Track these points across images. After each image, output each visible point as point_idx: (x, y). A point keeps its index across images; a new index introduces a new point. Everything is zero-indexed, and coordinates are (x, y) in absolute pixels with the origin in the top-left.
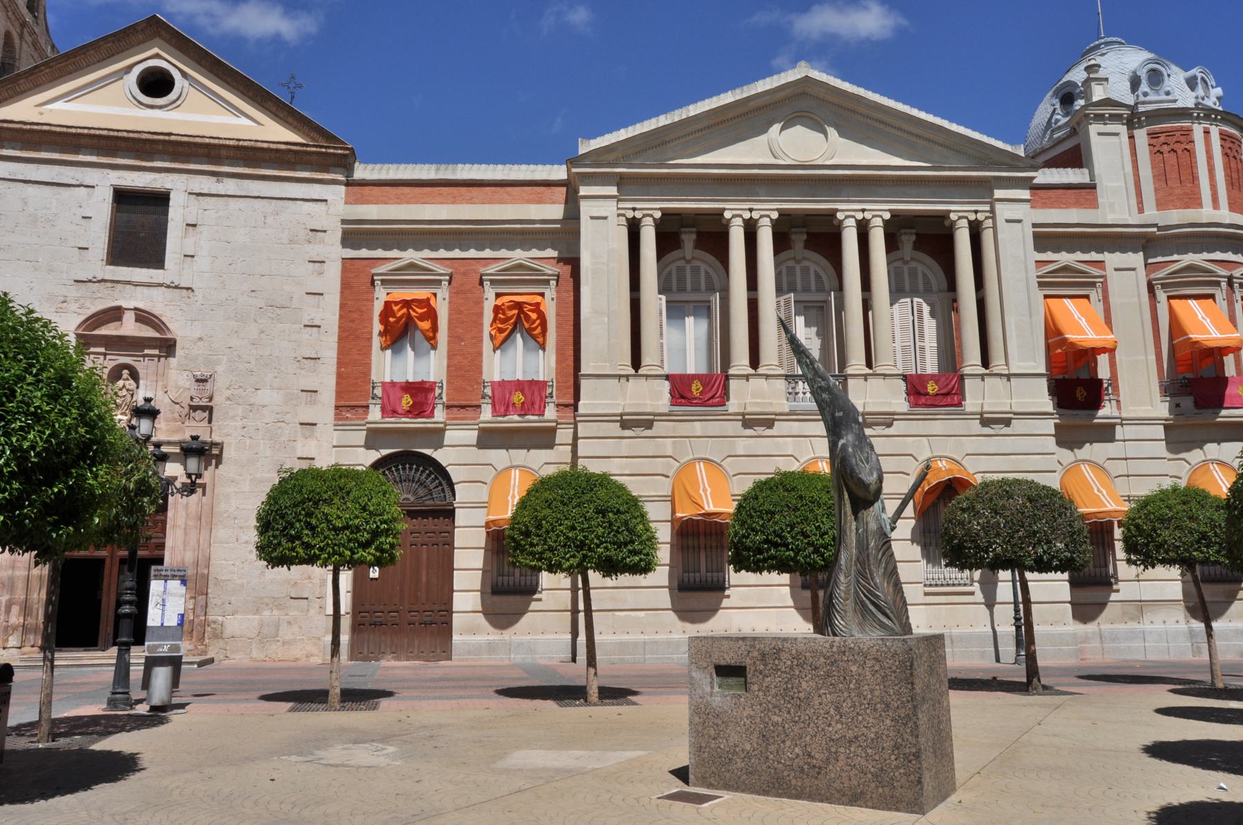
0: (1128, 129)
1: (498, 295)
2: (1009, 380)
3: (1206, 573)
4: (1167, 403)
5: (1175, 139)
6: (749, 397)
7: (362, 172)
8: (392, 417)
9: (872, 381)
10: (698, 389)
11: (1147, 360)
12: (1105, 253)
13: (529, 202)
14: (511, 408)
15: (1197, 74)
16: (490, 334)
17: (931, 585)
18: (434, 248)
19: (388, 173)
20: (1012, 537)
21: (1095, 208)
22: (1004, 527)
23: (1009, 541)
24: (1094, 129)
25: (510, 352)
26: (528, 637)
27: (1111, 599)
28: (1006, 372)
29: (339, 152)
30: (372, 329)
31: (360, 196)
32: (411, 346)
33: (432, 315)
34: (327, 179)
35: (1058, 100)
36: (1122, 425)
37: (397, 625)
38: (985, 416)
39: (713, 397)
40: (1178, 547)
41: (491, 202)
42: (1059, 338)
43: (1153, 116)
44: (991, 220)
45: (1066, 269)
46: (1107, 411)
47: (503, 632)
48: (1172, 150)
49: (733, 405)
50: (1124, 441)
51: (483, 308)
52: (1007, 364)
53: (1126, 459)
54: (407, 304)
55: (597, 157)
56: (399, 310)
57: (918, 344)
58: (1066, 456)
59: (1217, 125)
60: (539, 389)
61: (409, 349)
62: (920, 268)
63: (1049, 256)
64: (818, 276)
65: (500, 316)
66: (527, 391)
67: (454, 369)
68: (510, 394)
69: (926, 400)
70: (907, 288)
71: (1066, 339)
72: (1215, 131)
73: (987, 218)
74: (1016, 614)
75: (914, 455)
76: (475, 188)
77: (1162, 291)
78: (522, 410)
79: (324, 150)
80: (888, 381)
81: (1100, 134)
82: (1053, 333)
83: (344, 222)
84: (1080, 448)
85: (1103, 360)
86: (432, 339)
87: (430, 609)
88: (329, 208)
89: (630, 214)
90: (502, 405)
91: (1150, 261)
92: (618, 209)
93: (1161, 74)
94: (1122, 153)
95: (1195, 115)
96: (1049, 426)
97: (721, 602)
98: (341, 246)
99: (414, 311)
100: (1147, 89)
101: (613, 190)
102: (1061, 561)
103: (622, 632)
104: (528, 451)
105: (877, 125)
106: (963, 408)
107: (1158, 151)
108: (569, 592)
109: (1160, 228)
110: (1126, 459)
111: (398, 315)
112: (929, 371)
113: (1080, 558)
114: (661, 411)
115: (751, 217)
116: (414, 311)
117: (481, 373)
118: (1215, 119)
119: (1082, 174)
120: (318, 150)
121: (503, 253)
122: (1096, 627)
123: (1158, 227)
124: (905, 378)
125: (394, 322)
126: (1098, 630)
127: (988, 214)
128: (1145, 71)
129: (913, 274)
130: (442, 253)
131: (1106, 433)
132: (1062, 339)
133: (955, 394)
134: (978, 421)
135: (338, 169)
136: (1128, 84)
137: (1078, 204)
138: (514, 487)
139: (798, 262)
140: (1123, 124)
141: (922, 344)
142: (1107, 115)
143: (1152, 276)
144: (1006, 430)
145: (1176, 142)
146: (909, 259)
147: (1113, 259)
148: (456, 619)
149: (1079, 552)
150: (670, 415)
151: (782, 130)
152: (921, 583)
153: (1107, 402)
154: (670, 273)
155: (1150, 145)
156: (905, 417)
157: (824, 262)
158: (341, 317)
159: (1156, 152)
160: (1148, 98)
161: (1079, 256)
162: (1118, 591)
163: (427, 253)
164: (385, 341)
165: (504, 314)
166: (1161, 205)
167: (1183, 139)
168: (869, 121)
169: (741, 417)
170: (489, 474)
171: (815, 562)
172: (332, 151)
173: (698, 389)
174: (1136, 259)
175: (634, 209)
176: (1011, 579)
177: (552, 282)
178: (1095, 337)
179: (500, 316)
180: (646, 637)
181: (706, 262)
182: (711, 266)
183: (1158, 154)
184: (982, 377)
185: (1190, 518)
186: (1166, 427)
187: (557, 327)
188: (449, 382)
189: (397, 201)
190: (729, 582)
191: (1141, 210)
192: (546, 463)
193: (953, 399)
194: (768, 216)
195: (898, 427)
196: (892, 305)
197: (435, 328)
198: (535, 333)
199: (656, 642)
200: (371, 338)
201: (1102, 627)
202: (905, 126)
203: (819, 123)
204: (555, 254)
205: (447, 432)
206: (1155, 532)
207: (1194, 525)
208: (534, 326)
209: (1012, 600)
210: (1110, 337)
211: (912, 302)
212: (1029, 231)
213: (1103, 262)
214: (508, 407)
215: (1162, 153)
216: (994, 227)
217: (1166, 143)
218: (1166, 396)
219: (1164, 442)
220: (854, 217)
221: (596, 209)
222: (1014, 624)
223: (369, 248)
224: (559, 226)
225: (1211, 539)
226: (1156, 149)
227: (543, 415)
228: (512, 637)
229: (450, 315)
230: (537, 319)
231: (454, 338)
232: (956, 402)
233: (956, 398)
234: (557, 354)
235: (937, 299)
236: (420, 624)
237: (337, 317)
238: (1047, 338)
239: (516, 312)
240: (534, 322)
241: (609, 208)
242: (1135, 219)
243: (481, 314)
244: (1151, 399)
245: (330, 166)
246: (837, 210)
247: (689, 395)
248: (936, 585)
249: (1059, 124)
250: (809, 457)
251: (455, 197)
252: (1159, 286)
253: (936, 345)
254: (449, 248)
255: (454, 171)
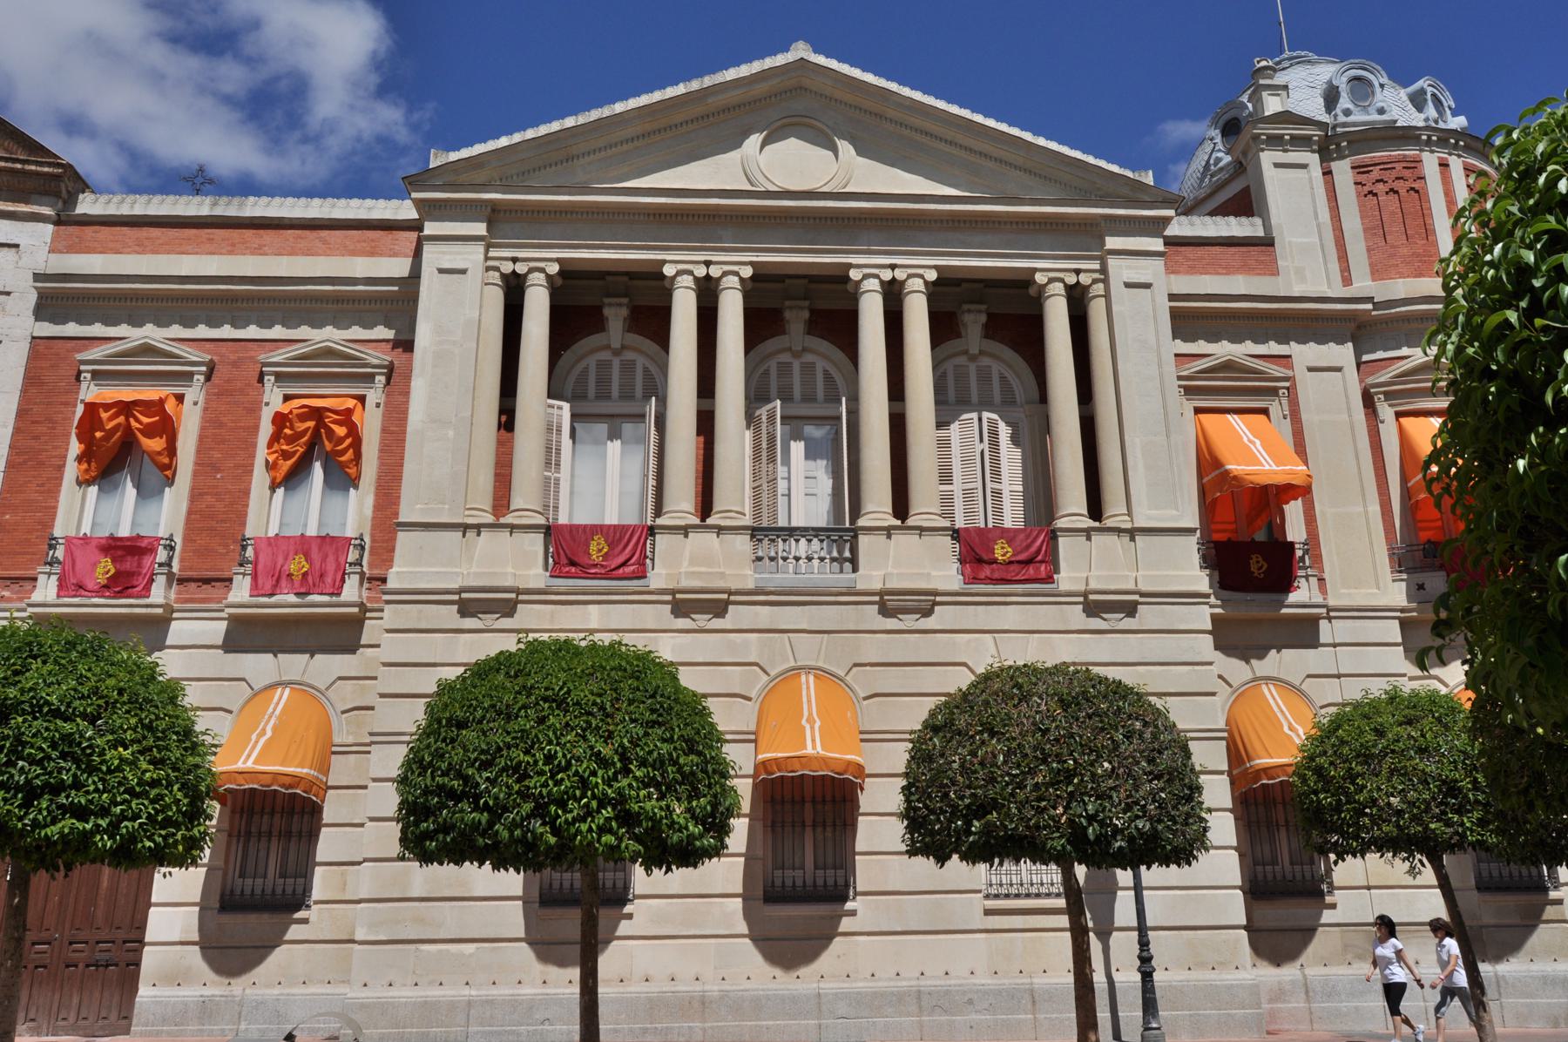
0: (1322, 161)
1: (287, 398)
2: (1133, 539)
3: (1485, 874)
4: (1404, 584)
5: (1394, 174)
6: (686, 563)
7: (87, 205)
8: (75, 596)
9: (900, 539)
10: (600, 551)
11: (1366, 512)
12: (1292, 343)
13: (354, 253)
14: (284, 582)
15: (1425, 86)
16: (267, 461)
17: (997, 896)
18: (189, 323)
19: (132, 207)
20: (1021, 786)
21: (1273, 275)
22: (1005, 762)
23: (1013, 795)
24: (1268, 158)
25: (299, 496)
26: (276, 991)
27: (1323, 921)
28: (1129, 526)
29: (46, 169)
30: (67, 450)
31: (77, 240)
32: (132, 481)
33: (167, 428)
34: (23, 212)
35: (1218, 131)
36: (1330, 619)
37: (45, 967)
38: (1092, 597)
39: (624, 564)
40: (1399, 813)
41: (293, 253)
42: (1217, 472)
43: (1359, 141)
44: (1101, 286)
45: (1228, 367)
46: (1303, 594)
47: (232, 982)
48: (1392, 190)
49: (658, 577)
50: (1335, 645)
51: (260, 418)
52: (1130, 514)
53: (1339, 676)
54: (126, 408)
55: (453, 176)
56: (111, 419)
57: (989, 485)
58: (1237, 670)
59: (1459, 156)
60: (337, 550)
61: (129, 484)
62: (996, 368)
63: (1200, 347)
64: (828, 377)
65: (287, 431)
66: (315, 555)
67: (197, 519)
68: (286, 559)
69: (993, 570)
70: (975, 398)
71: (1227, 472)
72: (1456, 164)
73: (1095, 281)
74: (1142, 950)
75: (970, 664)
76: (269, 231)
77: (1385, 405)
78: (302, 585)
79: (19, 166)
80: (928, 539)
81: (1277, 165)
82: (1208, 463)
83: (38, 277)
84: (1261, 657)
85: (1293, 511)
86: (167, 472)
87: (107, 938)
88: (20, 258)
89: (507, 267)
90: (269, 579)
91: (1365, 358)
92: (487, 258)
93: (1370, 84)
94: (1313, 195)
95: (1424, 137)
96: (1202, 616)
97: (615, 927)
98: (33, 318)
99: (137, 420)
100: (1350, 106)
101: (480, 229)
102: (1131, 840)
103: (431, 983)
104: (312, 656)
105: (918, 137)
106: (1054, 586)
107: (1370, 192)
108: (740, 900)
109: (1377, 306)
110: (1339, 676)
111: (108, 428)
112: (1008, 523)
113: (1175, 833)
114: (532, 585)
115: (1078, 282)
116: (137, 420)
117: (243, 524)
118: (1456, 146)
119: (1253, 225)
120: (10, 165)
121: (304, 332)
122: (1298, 972)
123: (1374, 304)
124: (956, 534)
125: (102, 439)
126: (1300, 977)
127: (1097, 276)
128: (1344, 79)
129: (984, 376)
130: (202, 331)
131: (1303, 633)
132: (1222, 473)
133: (1042, 562)
134: (1081, 607)
135: (45, 199)
136: (1321, 101)
137: (1246, 269)
138: (270, 717)
139: (796, 355)
140: (1313, 151)
141: (996, 486)
142: (1287, 137)
143: (1370, 380)
144: (1128, 623)
145: (1397, 178)
146: (977, 352)
147: (1305, 353)
148: (149, 957)
149: (1173, 819)
150: (545, 593)
151: (764, 144)
152: (980, 891)
153: (1304, 579)
154: (767, 373)
155: (1356, 183)
156: (955, 599)
157: (838, 355)
158: (17, 431)
159: (1367, 195)
160: (1351, 119)
161: (1250, 347)
162: (1333, 906)
163: (177, 331)
164: (87, 471)
165: (292, 428)
166: (1377, 272)
167: (1407, 173)
168: (907, 132)
169: (669, 598)
170: (236, 696)
171: (538, 838)
172: (33, 168)
173: (600, 551)
174: (1344, 354)
175: (515, 260)
176: (1132, 885)
177: (378, 378)
178: (1275, 468)
179: (287, 431)
180: (473, 993)
181: (822, 357)
182: (652, 359)
183: (1370, 196)
184: (1088, 533)
185: (1422, 751)
186: (1405, 625)
187: (381, 451)
188: (187, 539)
189: (137, 248)
190: (855, 888)
191: (1347, 281)
192: (340, 678)
193: (1038, 569)
194: (736, 274)
195: (943, 616)
196: (941, 424)
197: (171, 450)
198: (343, 459)
199: (490, 1002)
200: (64, 465)
201: (1308, 971)
202: (960, 138)
203: (827, 135)
204: (389, 334)
205: (174, 624)
206: (1353, 783)
207: (1431, 768)
208: (339, 448)
209: (1135, 923)
210: (1300, 468)
211: (980, 420)
212: (1165, 305)
213: (1290, 356)
214: (278, 580)
215: (1375, 195)
216: (1107, 296)
217: (1381, 180)
218: (1400, 572)
219: (1401, 648)
220: (876, 276)
221: (448, 257)
222: (1139, 970)
223: (80, 322)
224: (396, 288)
225: (1466, 796)
226: (1366, 189)
227: (339, 594)
228: (248, 991)
229: (203, 428)
230: (347, 436)
231: (204, 465)
232: (1043, 575)
233: (1043, 568)
234: (377, 495)
235: (1023, 416)
236: (88, 966)
237: (10, 430)
238: (1200, 476)
239: (311, 424)
240: (341, 440)
241: (472, 256)
242: (1339, 291)
243: (256, 428)
244: (1376, 576)
245: (32, 193)
246: (850, 266)
247: (584, 560)
248: (1007, 896)
249: (1221, 164)
250: (786, 666)
251: (233, 245)
252: (1382, 396)
253: (1020, 488)
254: (213, 323)
255: (241, 205)
